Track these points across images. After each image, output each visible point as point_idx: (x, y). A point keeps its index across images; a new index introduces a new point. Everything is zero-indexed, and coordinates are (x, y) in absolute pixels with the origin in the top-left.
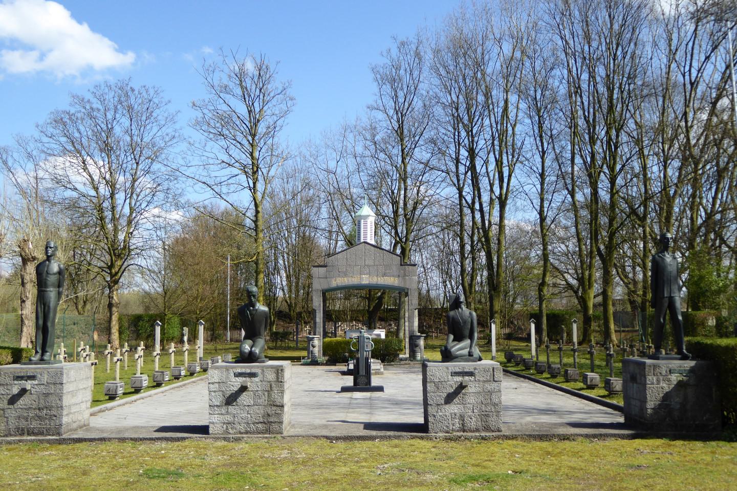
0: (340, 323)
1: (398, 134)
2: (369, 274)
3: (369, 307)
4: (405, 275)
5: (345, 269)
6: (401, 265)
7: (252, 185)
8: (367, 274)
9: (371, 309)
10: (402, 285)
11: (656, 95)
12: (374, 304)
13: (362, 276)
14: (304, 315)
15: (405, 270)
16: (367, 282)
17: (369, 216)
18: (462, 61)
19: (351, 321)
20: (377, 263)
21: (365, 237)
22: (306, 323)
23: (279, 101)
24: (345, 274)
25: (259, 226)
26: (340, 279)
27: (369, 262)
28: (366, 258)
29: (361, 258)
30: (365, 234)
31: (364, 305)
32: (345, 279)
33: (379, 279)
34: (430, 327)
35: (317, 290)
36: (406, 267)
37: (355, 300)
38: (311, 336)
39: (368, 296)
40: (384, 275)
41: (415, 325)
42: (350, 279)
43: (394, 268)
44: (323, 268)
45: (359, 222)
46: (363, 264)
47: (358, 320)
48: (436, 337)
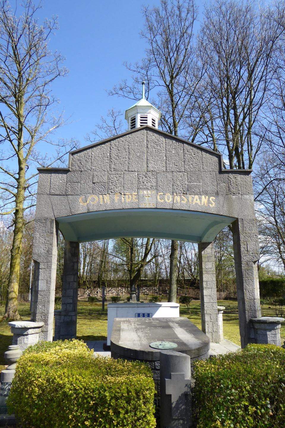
0: (110, 288)
3: (131, 277)
4: (229, 192)
5: (106, 178)
6: (221, 172)
11: (117, 295)
13: (141, 192)
14: (87, 283)
15: (229, 183)
18: (230, 56)
19: (118, 287)
22: (88, 288)
26: (96, 198)
29: (139, 157)
31: (127, 277)
32: (107, 198)
35: (46, 219)
36: (231, 176)
37: (120, 274)
38: (174, 287)
39: (130, 269)
42: (116, 198)
43: (208, 180)
44: (60, 175)
47: (123, 287)
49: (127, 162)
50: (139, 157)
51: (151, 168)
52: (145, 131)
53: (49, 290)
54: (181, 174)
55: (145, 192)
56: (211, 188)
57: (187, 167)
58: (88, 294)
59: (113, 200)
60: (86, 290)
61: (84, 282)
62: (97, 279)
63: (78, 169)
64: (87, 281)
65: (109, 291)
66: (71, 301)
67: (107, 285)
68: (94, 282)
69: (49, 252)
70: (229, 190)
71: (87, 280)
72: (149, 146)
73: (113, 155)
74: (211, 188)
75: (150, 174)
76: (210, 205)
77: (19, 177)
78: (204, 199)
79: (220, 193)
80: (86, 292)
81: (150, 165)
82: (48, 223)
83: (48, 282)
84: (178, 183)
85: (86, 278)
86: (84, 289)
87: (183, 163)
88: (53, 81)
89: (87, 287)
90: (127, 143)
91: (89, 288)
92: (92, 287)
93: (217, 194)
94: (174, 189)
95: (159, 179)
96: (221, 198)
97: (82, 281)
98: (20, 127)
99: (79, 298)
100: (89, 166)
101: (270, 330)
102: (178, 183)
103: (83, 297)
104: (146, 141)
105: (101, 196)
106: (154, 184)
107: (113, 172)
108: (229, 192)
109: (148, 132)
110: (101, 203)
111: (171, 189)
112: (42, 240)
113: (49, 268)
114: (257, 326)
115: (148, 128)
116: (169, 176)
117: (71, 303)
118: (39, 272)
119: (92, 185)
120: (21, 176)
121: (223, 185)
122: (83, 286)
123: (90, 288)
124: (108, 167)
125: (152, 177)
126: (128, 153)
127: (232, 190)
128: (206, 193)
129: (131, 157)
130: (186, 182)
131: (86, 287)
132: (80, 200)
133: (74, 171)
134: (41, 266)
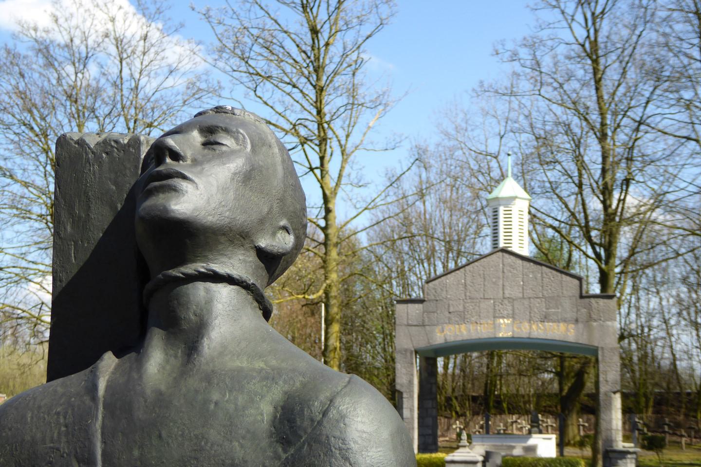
1: (585, 51)
2: (513, 316)
3: (561, 390)
4: (590, 318)
5: (461, 308)
6: (582, 297)
7: (316, 163)
8: (508, 317)
9: (564, 393)
10: (584, 340)
12: (569, 385)
14: (455, 403)
15: (589, 308)
16: (510, 334)
17: (515, 198)
20: (529, 293)
21: (508, 240)
22: (459, 416)
23: (366, 7)
24: (463, 317)
25: (331, 237)
26: (452, 327)
27: (513, 291)
28: (506, 284)
29: (494, 283)
30: (508, 233)
32: (463, 327)
33: (534, 327)
34: (678, 425)
35: (406, 350)
40: (545, 318)
41: (614, 426)
42: (472, 327)
43: (567, 304)
44: (416, 306)
45: (496, 212)
46: (501, 295)
48: (689, 445)
49: (482, 290)
50: (494, 283)
51: (507, 295)
52: (500, 254)
53: (412, 418)
54: (538, 300)
55: (501, 321)
56: (570, 315)
57: (545, 293)
58: (458, 430)
59: (469, 331)
60: (452, 421)
61: (448, 399)
62: (481, 392)
63: (433, 298)
64: (456, 398)
65: (512, 423)
66: (430, 432)
67: (509, 409)
68: (474, 399)
69: (411, 382)
70: (590, 317)
71: (456, 394)
72: (505, 271)
73: (468, 282)
74: (570, 315)
75: (506, 302)
76: (569, 333)
77: (327, 224)
78: (562, 326)
79: (580, 320)
80: (454, 427)
81: (506, 292)
82: (408, 354)
83: (412, 410)
84: (536, 310)
85: (453, 390)
86: (446, 417)
87: (541, 288)
88: (374, 37)
89: (457, 413)
90: (482, 268)
91: (462, 415)
92: (468, 413)
93: (577, 321)
94: (530, 317)
95: (516, 306)
96: (581, 326)
97: (443, 398)
98: (322, 134)
99: (441, 439)
100: (444, 294)
101: (621, 459)
102: (536, 310)
103: (447, 439)
104: (501, 265)
105: (457, 326)
106: (511, 312)
107: (469, 301)
108: (590, 318)
109: (504, 254)
110: (458, 333)
111: (528, 317)
112: (404, 371)
113: (412, 397)
114: (611, 455)
115: (504, 250)
116: (526, 302)
117: (430, 435)
118: (402, 401)
119: (447, 314)
120: (329, 223)
121: (584, 311)
122: (446, 411)
123: (464, 415)
124: (463, 295)
125: (508, 304)
126: (483, 280)
127: (593, 316)
128: (565, 321)
129: (486, 283)
130: (544, 310)
131: (454, 414)
132: (437, 331)
133: (429, 301)
134: (405, 395)
